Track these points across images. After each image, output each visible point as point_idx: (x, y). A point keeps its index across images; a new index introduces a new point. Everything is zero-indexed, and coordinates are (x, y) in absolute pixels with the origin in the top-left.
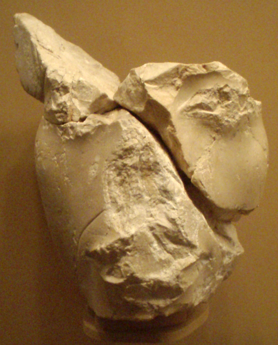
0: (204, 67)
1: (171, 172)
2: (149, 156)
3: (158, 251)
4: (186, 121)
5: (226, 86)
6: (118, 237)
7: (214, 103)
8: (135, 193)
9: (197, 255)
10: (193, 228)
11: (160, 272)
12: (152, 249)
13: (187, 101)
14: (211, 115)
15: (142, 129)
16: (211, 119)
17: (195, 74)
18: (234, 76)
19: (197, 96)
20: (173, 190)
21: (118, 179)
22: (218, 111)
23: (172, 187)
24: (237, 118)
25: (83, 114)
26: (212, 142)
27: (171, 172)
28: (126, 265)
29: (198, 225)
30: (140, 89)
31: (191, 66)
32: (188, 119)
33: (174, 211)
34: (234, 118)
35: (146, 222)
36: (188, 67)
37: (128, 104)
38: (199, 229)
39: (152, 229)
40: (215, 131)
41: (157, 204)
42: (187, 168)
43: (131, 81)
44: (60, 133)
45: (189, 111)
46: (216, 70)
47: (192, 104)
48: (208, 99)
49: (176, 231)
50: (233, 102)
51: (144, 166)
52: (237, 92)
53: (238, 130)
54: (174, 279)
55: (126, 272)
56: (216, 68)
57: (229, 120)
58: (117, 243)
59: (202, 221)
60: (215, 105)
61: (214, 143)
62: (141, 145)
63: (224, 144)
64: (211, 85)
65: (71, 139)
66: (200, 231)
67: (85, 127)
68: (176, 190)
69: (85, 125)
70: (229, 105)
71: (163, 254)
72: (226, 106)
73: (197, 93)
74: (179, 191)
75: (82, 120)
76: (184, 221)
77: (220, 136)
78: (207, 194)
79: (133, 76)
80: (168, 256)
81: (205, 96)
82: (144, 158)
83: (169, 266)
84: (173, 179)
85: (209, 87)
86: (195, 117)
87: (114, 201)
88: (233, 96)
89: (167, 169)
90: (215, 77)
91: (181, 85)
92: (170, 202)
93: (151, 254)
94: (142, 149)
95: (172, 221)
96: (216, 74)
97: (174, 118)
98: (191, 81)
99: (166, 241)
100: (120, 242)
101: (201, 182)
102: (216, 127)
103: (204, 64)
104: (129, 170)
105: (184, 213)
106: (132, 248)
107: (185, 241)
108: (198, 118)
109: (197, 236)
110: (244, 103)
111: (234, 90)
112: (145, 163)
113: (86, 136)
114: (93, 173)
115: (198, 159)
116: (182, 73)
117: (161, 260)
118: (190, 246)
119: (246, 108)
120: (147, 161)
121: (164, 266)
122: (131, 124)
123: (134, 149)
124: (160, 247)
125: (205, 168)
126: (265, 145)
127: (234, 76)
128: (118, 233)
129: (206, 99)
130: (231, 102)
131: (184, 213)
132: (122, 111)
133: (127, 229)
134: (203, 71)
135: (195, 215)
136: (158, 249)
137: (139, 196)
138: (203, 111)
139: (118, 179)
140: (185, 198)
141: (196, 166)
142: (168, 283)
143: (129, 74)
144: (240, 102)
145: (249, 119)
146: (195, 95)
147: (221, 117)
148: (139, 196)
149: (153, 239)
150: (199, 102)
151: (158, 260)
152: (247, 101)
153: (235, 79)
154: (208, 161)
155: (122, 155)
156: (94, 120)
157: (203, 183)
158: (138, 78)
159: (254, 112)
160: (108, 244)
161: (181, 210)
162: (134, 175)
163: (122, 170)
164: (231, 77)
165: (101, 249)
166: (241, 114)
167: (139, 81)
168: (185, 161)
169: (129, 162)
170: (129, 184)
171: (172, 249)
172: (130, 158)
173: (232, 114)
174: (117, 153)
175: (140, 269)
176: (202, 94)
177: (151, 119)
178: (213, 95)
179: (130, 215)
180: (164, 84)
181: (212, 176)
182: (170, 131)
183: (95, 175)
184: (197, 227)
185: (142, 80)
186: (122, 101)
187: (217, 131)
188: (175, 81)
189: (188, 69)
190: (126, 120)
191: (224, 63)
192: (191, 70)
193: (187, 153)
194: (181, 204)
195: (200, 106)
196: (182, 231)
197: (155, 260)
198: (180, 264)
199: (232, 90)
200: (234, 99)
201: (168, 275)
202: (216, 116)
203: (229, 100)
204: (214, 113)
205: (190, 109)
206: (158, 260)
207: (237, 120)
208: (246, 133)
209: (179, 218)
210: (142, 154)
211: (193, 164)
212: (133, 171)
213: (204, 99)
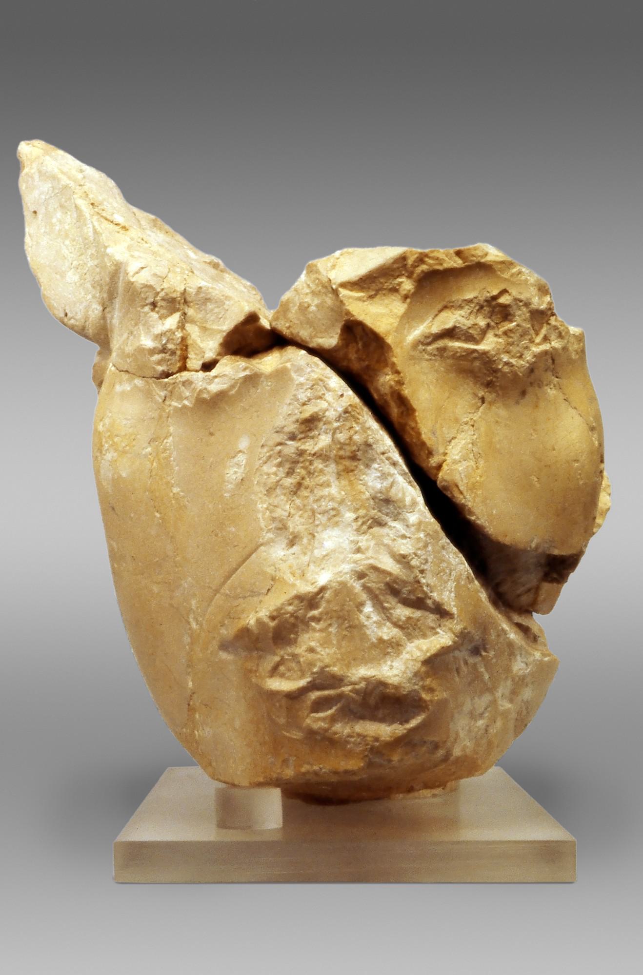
0: (459, 253)
1: (394, 464)
2: (352, 432)
3: (375, 622)
4: (425, 364)
5: (504, 292)
6: (294, 592)
7: (480, 327)
8: (323, 508)
9: (454, 634)
10: (445, 577)
11: (380, 664)
12: (362, 618)
13: (425, 325)
14: (475, 351)
15: (336, 382)
16: (475, 358)
17: (440, 268)
18: (520, 273)
19: (444, 314)
20: (402, 500)
21: (289, 481)
22: (489, 344)
23: (400, 495)
24: (528, 357)
25: (210, 355)
26: (479, 408)
27: (394, 464)
28: (312, 650)
29: (453, 573)
30: (329, 300)
31: (432, 252)
32: (427, 360)
33: (404, 541)
34: (521, 357)
35: (349, 563)
36: (426, 255)
37: (304, 334)
38: (457, 580)
39: (361, 576)
40: (482, 384)
41: (370, 527)
42: (428, 457)
43: (308, 286)
44: (160, 396)
45: (429, 344)
46: (483, 260)
47: (435, 329)
48: (468, 318)
49: (411, 579)
50: (518, 325)
51: (342, 453)
52: (527, 304)
53: (531, 384)
54: (409, 680)
55: (311, 664)
56: (482, 257)
57: (513, 361)
58: (290, 604)
59: (462, 567)
60: (484, 333)
61: (481, 409)
62: (335, 410)
63: (503, 412)
64: (475, 290)
65: (185, 407)
66: (458, 587)
67: (216, 380)
68: (408, 500)
69: (216, 377)
70: (511, 330)
71: (385, 630)
72: (505, 333)
73: (445, 307)
74: (414, 503)
75: (208, 367)
76: (426, 561)
77: (494, 395)
78: (471, 513)
79: (314, 276)
80: (395, 632)
81: (462, 312)
82: (342, 437)
83: (399, 654)
84: (400, 479)
85: (469, 296)
86: (442, 356)
87: (281, 526)
88: (519, 313)
89: (388, 459)
90: (481, 274)
91: (413, 291)
92: (397, 525)
93: (361, 626)
94: (338, 420)
95: (402, 559)
96: (482, 268)
97: (398, 357)
98: (433, 283)
99: (391, 602)
100: (296, 602)
101: (457, 486)
102: (486, 377)
103: (458, 248)
104: (311, 463)
105: (426, 546)
106: (321, 613)
107: (429, 602)
108: (448, 358)
109: (453, 595)
110: (541, 328)
111: (521, 301)
112: (342, 446)
113: (221, 396)
114: (236, 472)
115: (450, 442)
116: (415, 266)
117: (381, 640)
118: (441, 612)
119: (546, 339)
120: (347, 442)
121: (388, 653)
122: (313, 371)
123: (319, 420)
124: (379, 614)
125: (465, 458)
126: (592, 419)
127: (520, 273)
128: (294, 585)
129: (463, 320)
130: (514, 324)
131: (426, 546)
132: (291, 351)
133: (309, 576)
134: (455, 262)
135: (448, 553)
136: (375, 618)
137: (332, 513)
138: (457, 344)
139: (289, 481)
140: (425, 517)
141: (445, 454)
142: (396, 687)
143: (304, 272)
144: (533, 326)
145: (553, 360)
146: (440, 311)
147: (495, 355)
148: (332, 513)
149: (364, 596)
150: (449, 325)
151: (374, 640)
152: (549, 324)
153: (523, 278)
154: (470, 446)
155: (297, 432)
156: (232, 369)
157: (461, 488)
158: (325, 280)
159: (565, 349)
160: (272, 608)
161: (419, 539)
162: (321, 471)
163: (296, 462)
164: (512, 275)
165: (259, 622)
166: (536, 349)
167: (327, 284)
168: (423, 444)
169: (309, 446)
170: (312, 491)
171: (404, 619)
172: (313, 438)
173: (518, 349)
174: (286, 430)
175: (339, 656)
176: (456, 309)
177: (354, 358)
178: (478, 310)
179: (316, 551)
180: (377, 291)
181: (481, 477)
182: (393, 383)
183: (239, 476)
184: (453, 578)
185: (333, 282)
186: (288, 328)
187: (489, 385)
188: (400, 284)
189: (427, 259)
190: (302, 363)
191: (499, 246)
192: (431, 262)
193: (427, 426)
194: (419, 525)
195: (450, 333)
196: (423, 581)
197: (369, 640)
198: (421, 650)
199: (517, 300)
200: (521, 318)
201: (395, 672)
202: (485, 353)
203: (511, 321)
204: (481, 347)
205: (430, 340)
206: (374, 640)
207: (528, 362)
208: (549, 390)
209: (415, 554)
210: (337, 428)
211: (441, 450)
212: (318, 464)
213: (459, 318)
